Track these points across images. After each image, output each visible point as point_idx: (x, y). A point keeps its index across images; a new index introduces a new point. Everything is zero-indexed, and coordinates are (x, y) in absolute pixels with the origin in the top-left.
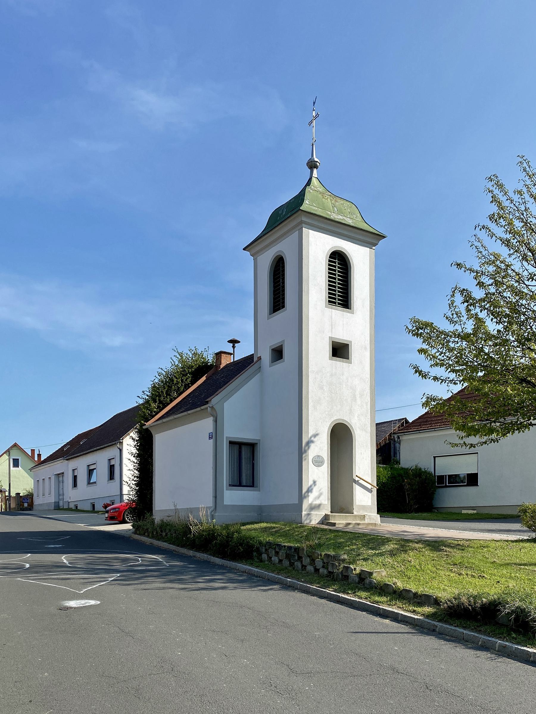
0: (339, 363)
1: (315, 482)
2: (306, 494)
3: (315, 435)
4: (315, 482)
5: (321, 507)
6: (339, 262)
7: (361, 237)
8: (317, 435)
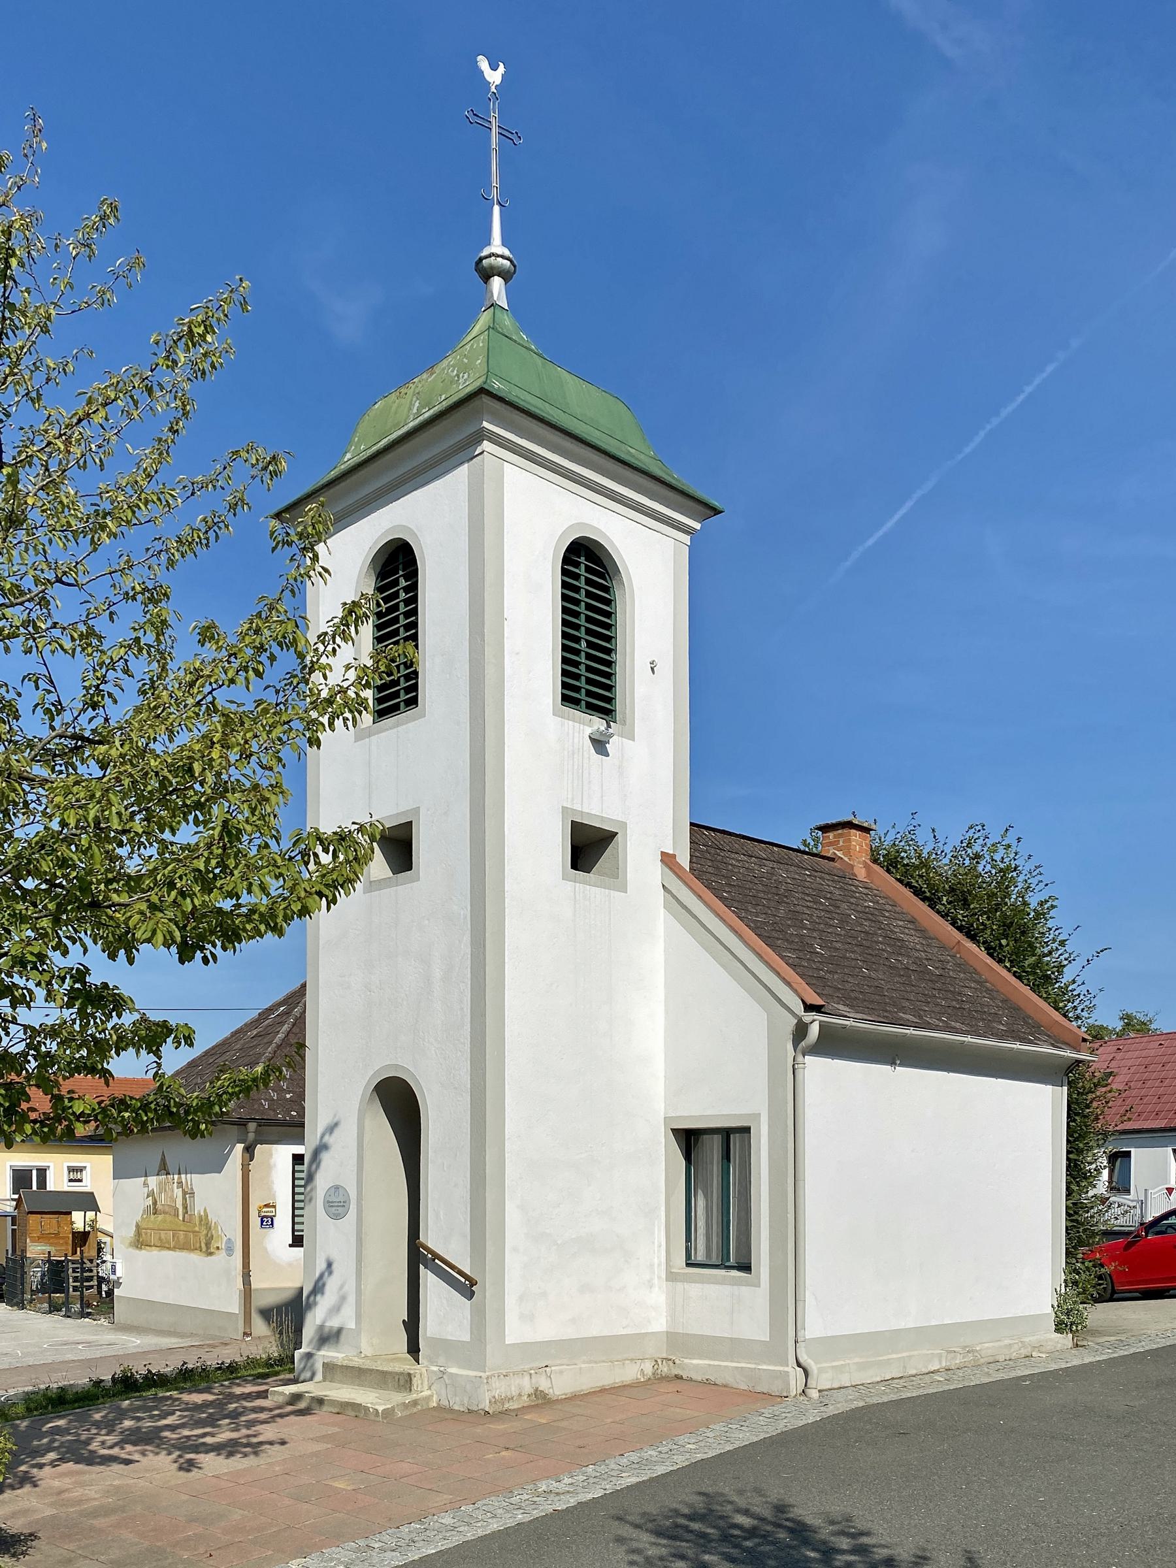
0: (587, 890)
1: (329, 1265)
2: (312, 1298)
3: (332, 1128)
4: (329, 1265)
5: (343, 1337)
6: (587, 573)
7: (436, 450)
8: (336, 1125)
